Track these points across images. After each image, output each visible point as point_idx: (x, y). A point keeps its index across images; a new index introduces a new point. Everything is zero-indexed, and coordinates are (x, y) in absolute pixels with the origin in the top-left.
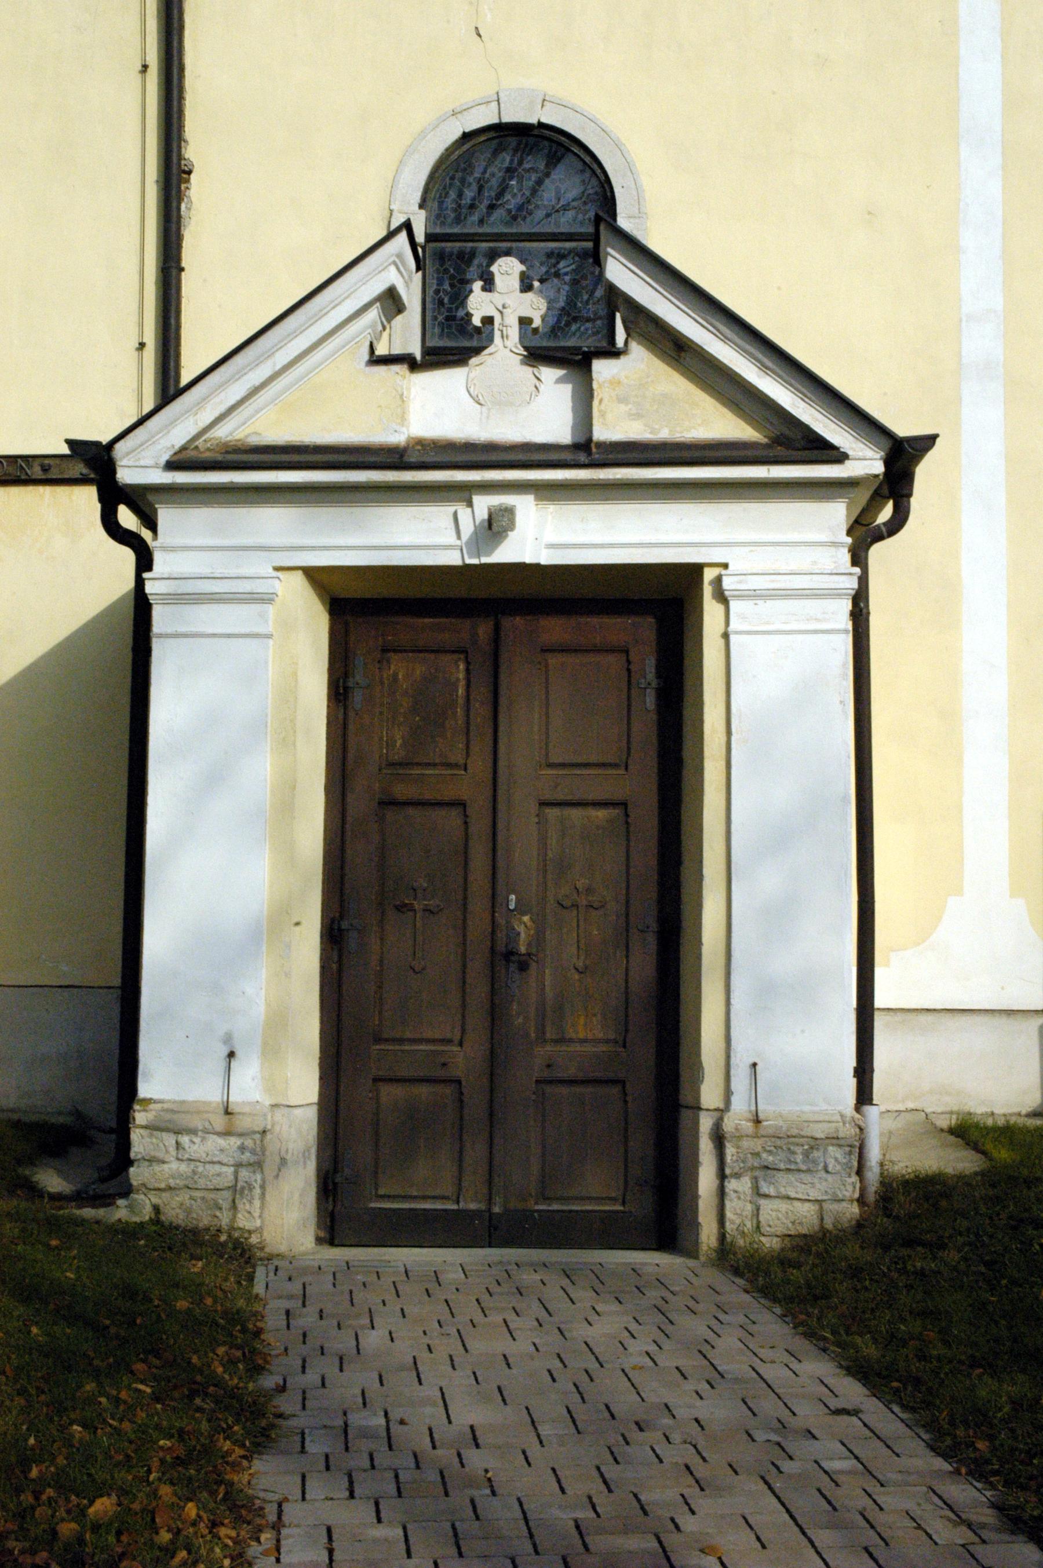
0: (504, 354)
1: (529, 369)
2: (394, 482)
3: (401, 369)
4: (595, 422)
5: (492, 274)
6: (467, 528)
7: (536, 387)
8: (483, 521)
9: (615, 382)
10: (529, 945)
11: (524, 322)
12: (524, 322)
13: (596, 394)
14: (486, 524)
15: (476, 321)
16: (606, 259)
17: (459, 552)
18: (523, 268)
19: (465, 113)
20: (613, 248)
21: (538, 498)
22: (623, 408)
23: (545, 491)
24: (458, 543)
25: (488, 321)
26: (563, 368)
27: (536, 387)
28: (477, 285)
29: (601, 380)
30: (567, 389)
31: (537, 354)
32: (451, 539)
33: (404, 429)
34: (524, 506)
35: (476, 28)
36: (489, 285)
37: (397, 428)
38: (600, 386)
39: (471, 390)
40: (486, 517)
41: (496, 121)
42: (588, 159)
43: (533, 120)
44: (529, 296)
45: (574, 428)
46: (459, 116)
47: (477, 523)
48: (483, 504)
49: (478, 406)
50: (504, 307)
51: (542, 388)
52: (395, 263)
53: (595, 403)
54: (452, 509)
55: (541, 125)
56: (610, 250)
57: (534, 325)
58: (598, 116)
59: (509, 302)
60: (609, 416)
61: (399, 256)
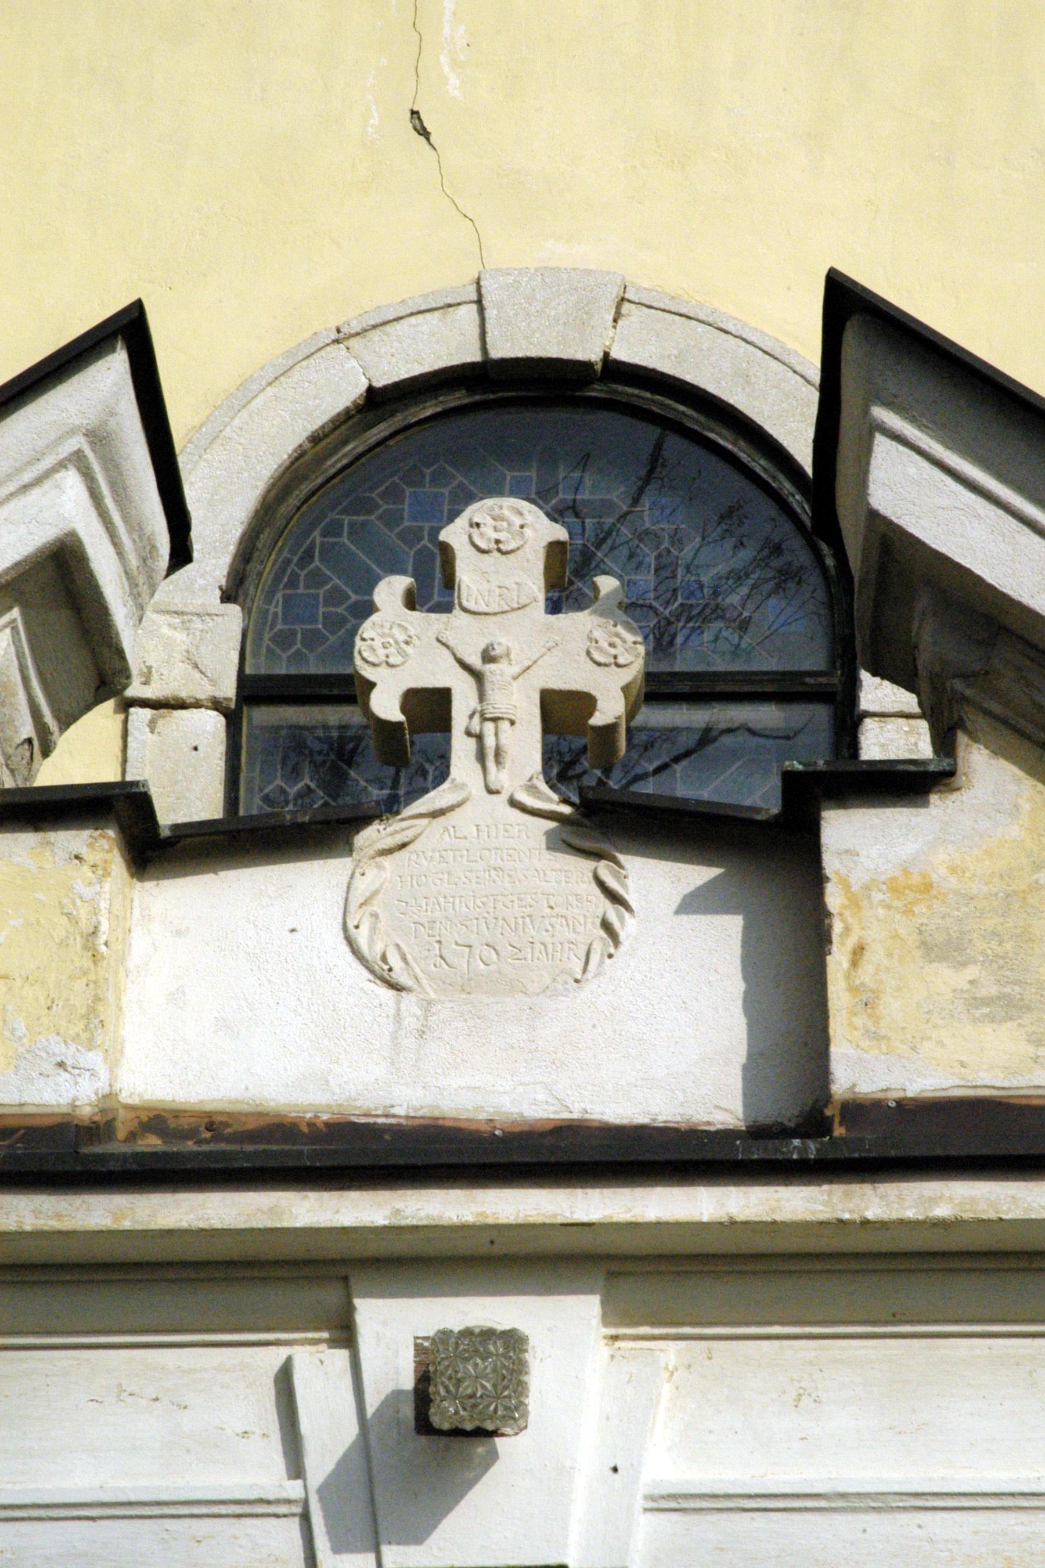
0: (483, 827)
1: (584, 866)
2: (38, 1235)
3: (98, 846)
4: (837, 1027)
5: (446, 552)
6: (331, 1428)
7: (606, 926)
8: (397, 1394)
9: (911, 888)
10: (566, 801)
11: (563, 713)
12: (563, 713)
13: (837, 927)
14: (408, 1411)
15: (386, 705)
16: (866, 452)
17: (293, 1528)
18: (561, 533)
19: (375, 335)
20: (889, 404)
21: (616, 1314)
22: (946, 979)
23: (656, 1284)
24: (294, 1489)
25: (430, 707)
26: (709, 863)
27: (606, 926)
28: (390, 591)
29: (858, 879)
30: (727, 931)
31: (608, 798)
32: (263, 1472)
33: (94, 1059)
34: (562, 1334)
35: (414, 113)
36: (435, 587)
37: (69, 1053)
38: (854, 903)
39: (362, 938)
40: (408, 1382)
41: (473, 356)
42: (760, 465)
43: (590, 353)
44: (579, 623)
45: (753, 1072)
46: (352, 343)
47: (372, 1403)
48: (394, 1329)
49: (386, 994)
50: (488, 657)
51: (628, 927)
52: (77, 459)
53: (837, 961)
54: (272, 1358)
55: (615, 370)
56: (881, 414)
57: (598, 720)
58: (791, 345)
59: (503, 641)
60: (892, 1007)
61: (99, 438)
